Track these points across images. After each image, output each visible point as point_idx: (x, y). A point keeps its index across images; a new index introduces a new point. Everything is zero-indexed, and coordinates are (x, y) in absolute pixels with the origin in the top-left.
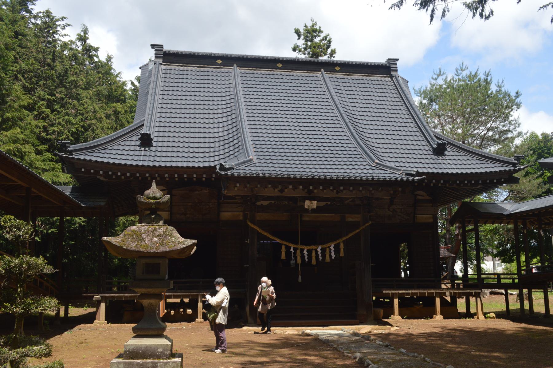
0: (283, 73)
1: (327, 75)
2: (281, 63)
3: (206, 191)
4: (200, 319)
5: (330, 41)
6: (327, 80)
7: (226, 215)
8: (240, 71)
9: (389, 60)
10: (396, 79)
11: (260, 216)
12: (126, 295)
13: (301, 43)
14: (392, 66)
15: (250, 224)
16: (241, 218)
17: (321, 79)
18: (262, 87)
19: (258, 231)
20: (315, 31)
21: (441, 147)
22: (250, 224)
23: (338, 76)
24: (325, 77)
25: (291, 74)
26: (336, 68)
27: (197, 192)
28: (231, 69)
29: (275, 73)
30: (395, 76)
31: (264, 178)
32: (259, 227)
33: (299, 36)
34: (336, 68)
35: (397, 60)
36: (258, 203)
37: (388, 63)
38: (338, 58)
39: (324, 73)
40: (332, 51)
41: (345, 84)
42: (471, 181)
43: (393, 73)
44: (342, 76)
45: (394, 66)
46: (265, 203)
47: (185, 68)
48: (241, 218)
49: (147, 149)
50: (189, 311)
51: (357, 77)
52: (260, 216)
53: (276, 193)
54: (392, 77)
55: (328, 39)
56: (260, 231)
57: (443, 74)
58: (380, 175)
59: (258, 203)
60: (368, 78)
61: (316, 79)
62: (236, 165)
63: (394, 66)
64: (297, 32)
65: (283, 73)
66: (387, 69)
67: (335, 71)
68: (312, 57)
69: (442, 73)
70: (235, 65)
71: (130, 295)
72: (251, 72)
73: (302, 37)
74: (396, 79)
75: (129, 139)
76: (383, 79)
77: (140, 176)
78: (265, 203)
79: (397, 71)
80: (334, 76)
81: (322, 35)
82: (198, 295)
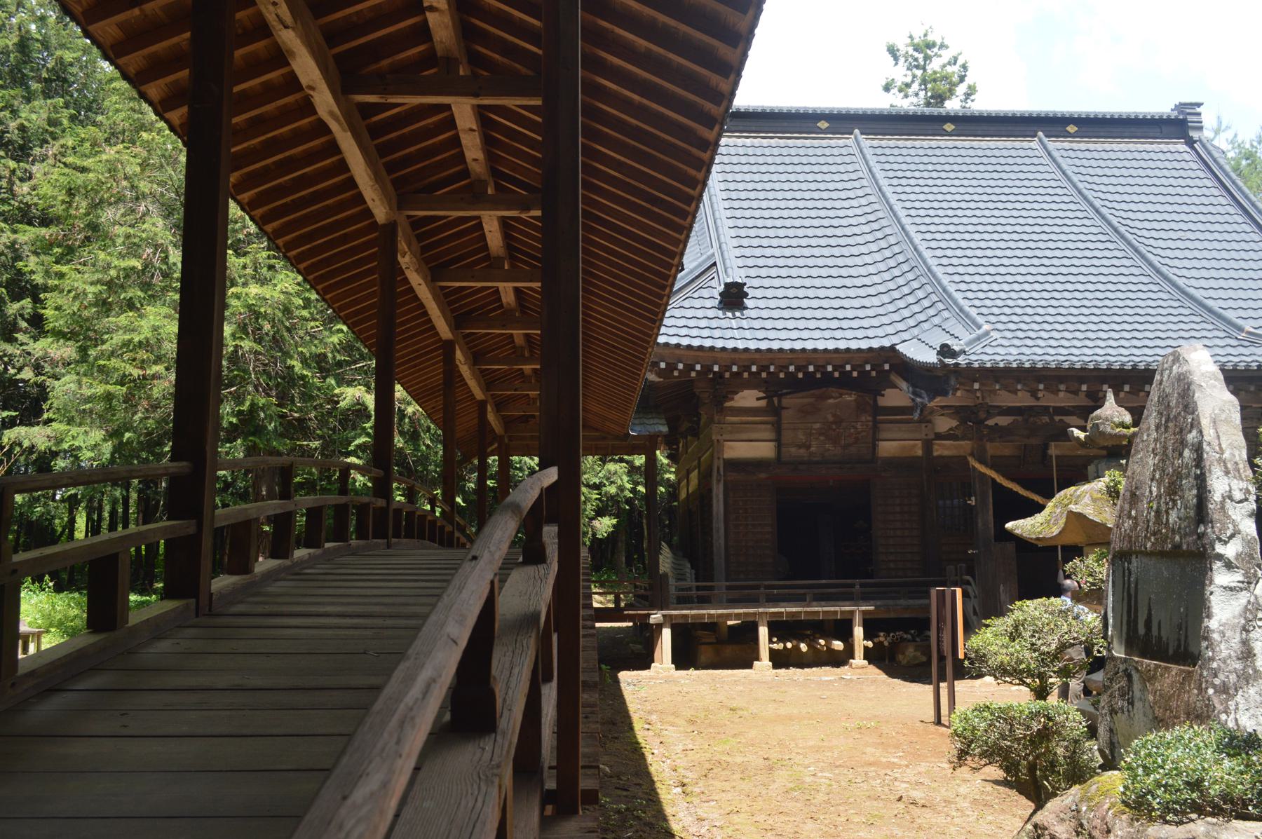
0: (958, 144)
1: (866, 142)
2: (1075, 124)
3: (850, 398)
4: (859, 660)
5: (964, 67)
6: (869, 153)
7: (888, 448)
8: (869, 143)
9: (1181, 107)
10: (1204, 146)
11: (992, 449)
12: (713, 612)
13: (900, 74)
14: (1190, 118)
15: (977, 465)
16: (920, 453)
17: (855, 150)
18: (737, 168)
19: (994, 480)
20: (930, 46)
21: (734, 290)
22: (977, 465)
23: (1075, 146)
24: (863, 145)
25: (975, 144)
26: (1068, 129)
27: (831, 401)
28: (850, 140)
29: (942, 144)
30: (1200, 141)
31: (1033, 369)
32: (997, 471)
33: (896, 58)
34: (1068, 129)
35: (1199, 105)
36: (990, 422)
37: (1181, 112)
38: (983, 104)
39: (861, 138)
40: (970, 87)
41: (900, 159)
42: (750, 368)
43: (1195, 135)
44: (1083, 146)
45: (1194, 118)
46: (1003, 421)
47: (757, 142)
48: (920, 453)
49: (738, 314)
50: (838, 645)
51: (1115, 147)
52: (992, 449)
53: (1022, 399)
54: (1191, 143)
55: (960, 62)
56: (1000, 480)
57: (1228, 128)
58: (1024, 358)
59: (990, 422)
60: (1140, 147)
61: (1030, 153)
62: (969, 343)
63: (1194, 118)
64: (893, 51)
65: (958, 144)
66: (1177, 126)
67: (1069, 135)
68: (928, 104)
69: (1223, 127)
70: (857, 131)
71: (720, 611)
72: (892, 143)
73: (902, 60)
74: (1204, 146)
75: (696, 295)
76: (1171, 147)
77: (872, 369)
78: (1003, 421)
79: (1201, 128)
80: (1067, 145)
81: (946, 55)
82: (852, 612)
